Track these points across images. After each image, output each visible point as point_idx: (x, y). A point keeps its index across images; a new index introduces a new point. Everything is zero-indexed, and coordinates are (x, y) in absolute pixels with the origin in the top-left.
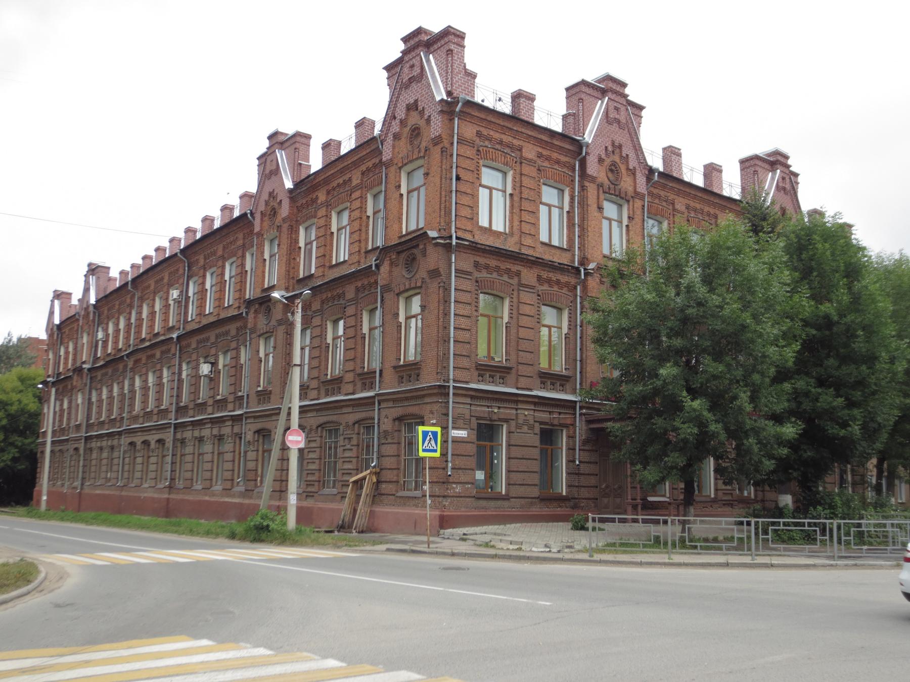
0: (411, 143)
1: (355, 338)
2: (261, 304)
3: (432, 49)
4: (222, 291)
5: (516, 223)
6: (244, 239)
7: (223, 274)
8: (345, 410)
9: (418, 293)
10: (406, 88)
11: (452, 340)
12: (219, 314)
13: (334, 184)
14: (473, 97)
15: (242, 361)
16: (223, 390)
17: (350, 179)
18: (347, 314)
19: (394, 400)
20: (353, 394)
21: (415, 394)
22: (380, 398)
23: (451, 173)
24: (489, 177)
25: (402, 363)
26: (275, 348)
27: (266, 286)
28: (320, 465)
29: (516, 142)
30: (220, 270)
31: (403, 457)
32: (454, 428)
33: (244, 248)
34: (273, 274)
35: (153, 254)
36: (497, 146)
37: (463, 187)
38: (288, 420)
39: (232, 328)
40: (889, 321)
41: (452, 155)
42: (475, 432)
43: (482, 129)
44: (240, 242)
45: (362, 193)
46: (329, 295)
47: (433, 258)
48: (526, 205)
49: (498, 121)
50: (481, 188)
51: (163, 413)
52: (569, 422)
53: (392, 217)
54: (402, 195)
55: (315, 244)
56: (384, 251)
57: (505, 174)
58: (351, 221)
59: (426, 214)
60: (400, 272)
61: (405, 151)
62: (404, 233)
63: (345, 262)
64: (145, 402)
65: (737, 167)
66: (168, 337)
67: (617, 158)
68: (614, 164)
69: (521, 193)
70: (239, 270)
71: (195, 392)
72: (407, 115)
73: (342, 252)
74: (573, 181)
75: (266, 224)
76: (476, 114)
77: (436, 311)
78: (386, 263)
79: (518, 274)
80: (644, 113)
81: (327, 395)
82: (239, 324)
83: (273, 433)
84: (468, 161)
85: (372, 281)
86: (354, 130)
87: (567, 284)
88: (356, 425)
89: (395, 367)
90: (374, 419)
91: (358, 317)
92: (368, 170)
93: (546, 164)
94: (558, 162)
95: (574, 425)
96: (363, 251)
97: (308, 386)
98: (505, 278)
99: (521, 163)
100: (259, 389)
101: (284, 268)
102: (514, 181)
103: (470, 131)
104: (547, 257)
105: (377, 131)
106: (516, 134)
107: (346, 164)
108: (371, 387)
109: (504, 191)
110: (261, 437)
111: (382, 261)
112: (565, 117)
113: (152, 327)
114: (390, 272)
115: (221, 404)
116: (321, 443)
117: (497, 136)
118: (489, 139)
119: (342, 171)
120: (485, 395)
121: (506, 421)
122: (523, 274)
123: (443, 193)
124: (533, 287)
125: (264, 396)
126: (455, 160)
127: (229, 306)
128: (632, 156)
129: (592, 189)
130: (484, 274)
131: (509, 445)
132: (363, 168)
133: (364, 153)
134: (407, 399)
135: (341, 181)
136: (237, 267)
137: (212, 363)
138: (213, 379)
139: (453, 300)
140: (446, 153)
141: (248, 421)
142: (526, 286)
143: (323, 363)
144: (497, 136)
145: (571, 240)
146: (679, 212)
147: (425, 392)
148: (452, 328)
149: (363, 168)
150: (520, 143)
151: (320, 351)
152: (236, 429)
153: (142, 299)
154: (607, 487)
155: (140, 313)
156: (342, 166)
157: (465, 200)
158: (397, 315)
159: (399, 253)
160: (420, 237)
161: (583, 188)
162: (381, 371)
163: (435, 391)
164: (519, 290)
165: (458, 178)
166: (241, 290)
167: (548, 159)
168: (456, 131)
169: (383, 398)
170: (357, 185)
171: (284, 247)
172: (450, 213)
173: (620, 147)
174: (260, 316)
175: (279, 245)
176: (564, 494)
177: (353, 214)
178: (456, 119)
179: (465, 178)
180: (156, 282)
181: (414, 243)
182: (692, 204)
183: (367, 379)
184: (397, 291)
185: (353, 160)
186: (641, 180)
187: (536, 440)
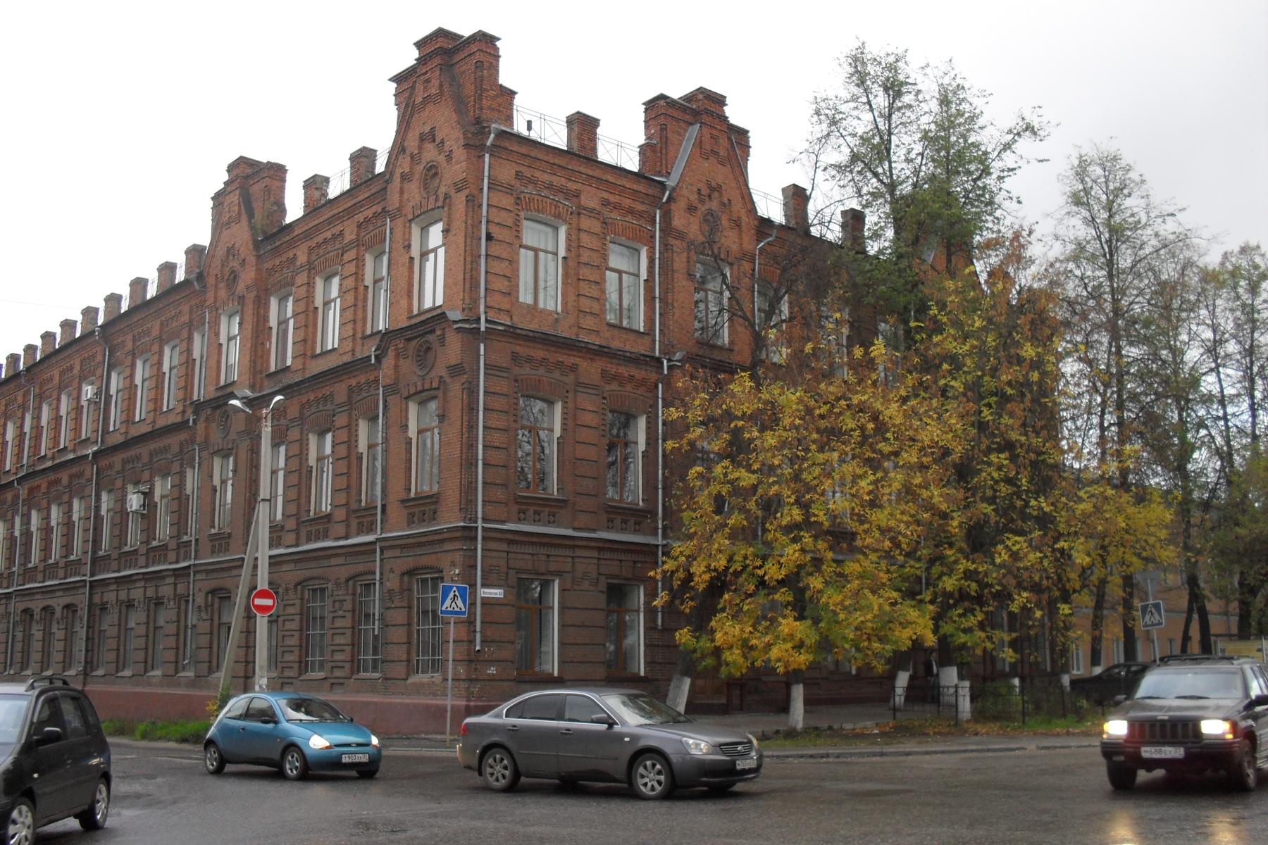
0: (426, 186)
1: (348, 460)
4: (159, 387)
5: (571, 298)
6: (191, 313)
7: (160, 363)
8: (334, 561)
9: (434, 397)
11: (480, 463)
12: (154, 422)
13: (319, 239)
14: (512, 125)
15: (189, 491)
16: (164, 530)
17: (341, 234)
18: (290, 438)
19: (402, 547)
20: (346, 538)
21: (430, 538)
22: (383, 544)
23: (480, 230)
24: (532, 234)
25: (412, 495)
26: (235, 471)
27: (222, 383)
28: (301, 639)
29: (572, 186)
30: (185, 344)
31: (415, 627)
32: (484, 585)
33: (191, 327)
35: (58, 331)
37: (496, 250)
38: (254, 575)
39: (174, 441)
41: (480, 206)
42: (515, 591)
43: (522, 169)
44: (185, 318)
45: (358, 254)
46: (312, 398)
47: (453, 349)
48: (586, 272)
50: (522, 251)
51: (72, 567)
53: (407, 286)
54: (412, 259)
55: (291, 322)
56: (387, 337)
57: (556, 229)
58: (343, 293)
59: (445, 286)
60: (408, 367)
61: (418, 198)
62: (416, 312)
63: (334, 350)
64: (46, 549)
66: (79, 454)
67: (714, 205)
69: (579, 256)
70: (184, 359)
71: (121, 536)
72: (420, 148)
73: (332, 334)
74: (653, 237)
75: (223, 293)
76: (516, 148)
77: (459, 423)
79: (574, 368)
81: (309, 540)
82: (183, 436)
83: (233, 595)
84: (503, 214)
85: (372, 378)
86: (348, 164)
87: (642, 383)
88: (351, 583)
89: (403, 501)
90: (374, 573)
91: (351, 429)
92: (367, 220)
93: (615, 215)
94: (631, 211)
96: (359, 335)
97: (283, 527)
98: (557, 374)
99: (579, 214)
100: (213, 531)
101: (248, 357)
102: (568, 239)
103: (506, 173)
104: (616, 344)
105: (380, 167)
107: (335, 211)
108: (370, 529)
109: (556, 254)
110: (217, 600)
112: (643, 150)
113: (56, 440)
114: (396, 366)
115: (159, 553)
116: (302, 609)
117: (546, 177)
118: (532, 181)
119: (330, 221)
120: (526, 539)
121: (559, 574)
123: (469, 259)
124: (596, 387)
125: (221, 541)
126: (484, 213)
127: (169, 411)
130: (526, 370)
131: (563, 608)
134: (420, 545)
135: (328, 235)
136: (181, 353)
137: (143, 493)
138: (148, 514)
139: (481, 408)
140: (473, 202)
141: (199, 577)
142: (586, 386)
143: (303, 495)
144: (546, 177)
145: (650, 320)
147: (446, 536)
148: (480, 447)
149: (360, 217)
150: (578, 186)
151: (300, 478)
152: (181, 589)
153: (41, 398)
155: (37, 418)
156: (331, 214)
158: (405, 427)
159: (409, 340)
160: (437, 318)
161: (665, 246)
162: (384, 506)
163: (458, 534)
164: (576, 391)
165: (489, 237)
166: (187, 387)
167: (616, 207)
168: (486, 174)
169: (387, 544)
170: (351, 242)
171: (249, 327)
172: (478, 286)
174: (214, 425)
175: (240, 324)
176: (642, 673)
177: (345, 283)
178: (487, 156)
179: (500, 238)
180: (62, 373)
181: (427, 327)
183: (363, 517)
184: (405, 394)
187: (601, 601)
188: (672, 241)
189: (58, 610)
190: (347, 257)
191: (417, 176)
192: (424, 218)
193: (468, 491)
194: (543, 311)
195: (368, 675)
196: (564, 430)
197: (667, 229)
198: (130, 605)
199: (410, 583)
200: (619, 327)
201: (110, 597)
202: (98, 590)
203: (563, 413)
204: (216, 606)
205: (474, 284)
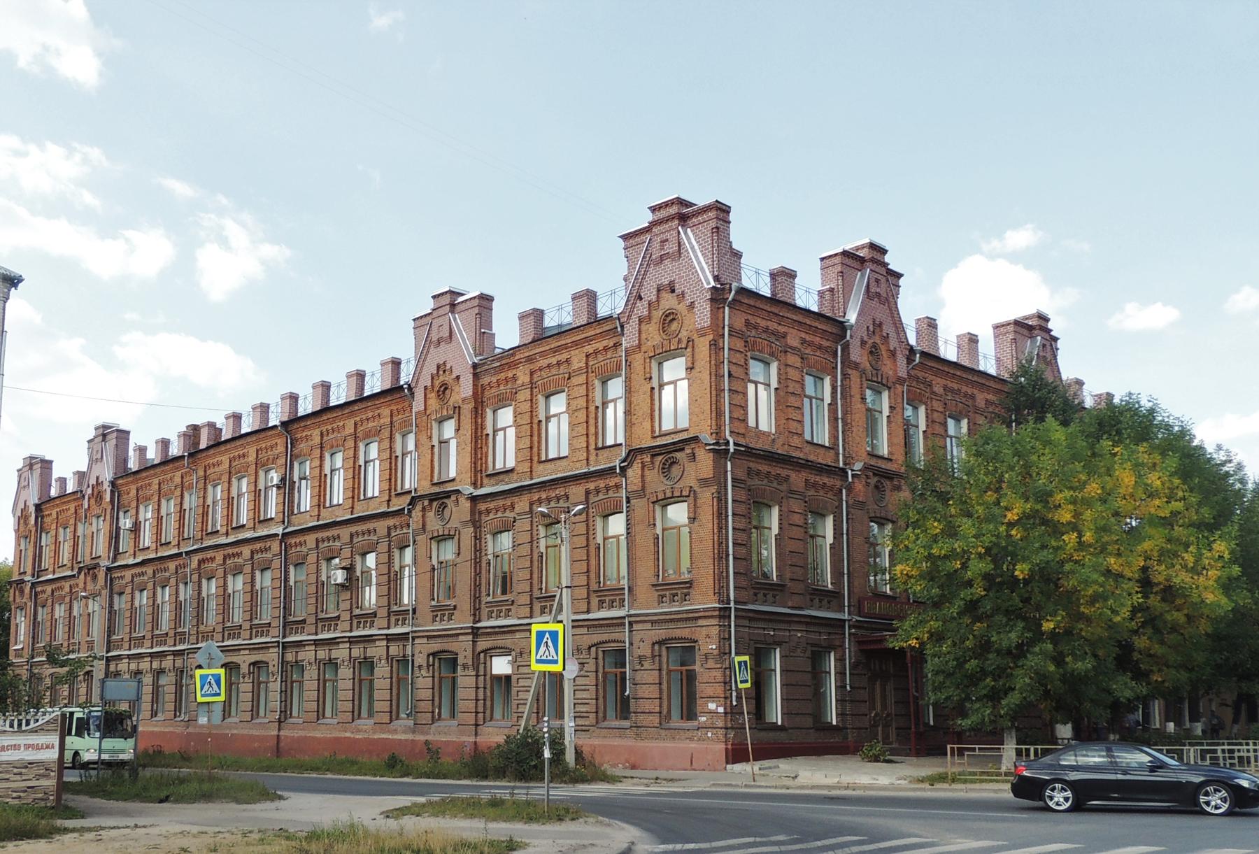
2: (431, 501)
3: (690, 222)
10: (656, 265)
29: (781, 329)
32: (737, 654)
34: (454, 466)
36: (764, 336)
40: (1094, 489)
43: (750, 317)
48: (792, 400)
49: (765, 307)
52: (838, 643)
58: (571, 411)
65: (991, 332)
67: (877, 339)
68: (874, 345)
78: (637, 466)
79: (787, 479)
80: (902, 281)
94: (820, 347)
95: (842, 646)
100: (434, 603)
106: (781, 319)
111: (630, 465)
112: (821, 294)
117: (763, 323)
122: (791, 480)
124: (800, 493)
128: (893, 335)
129: (854, 375)
132: (589, 349)
133: (593, 333)
139: (730, 513)
144: (763, 323)
145: (834, 437)
146: (936, 394)
149: (589, 349)
154: (876, 715)
157: (738, 399)
159: (653, 456)
161: (845, 376)
173: (880, 325)
182: (950, 385)
185: (574, 339)
186: (902, 361)
188: (850, 372)
189: (244, 669)
190: (574, 381)
191: (654, 321)
192: (663, 355)
193: (721, 578)
194: (764, 433)
195: (329, 721)
196: (780, 528)
197: (847, 362)
198: (333, 664)
199: (660, 650)
200: (811, 443)
201: (307, 655)
202: (289, 650)
203: (780, 515)
204: (437, 665)
205: (719, 413)
